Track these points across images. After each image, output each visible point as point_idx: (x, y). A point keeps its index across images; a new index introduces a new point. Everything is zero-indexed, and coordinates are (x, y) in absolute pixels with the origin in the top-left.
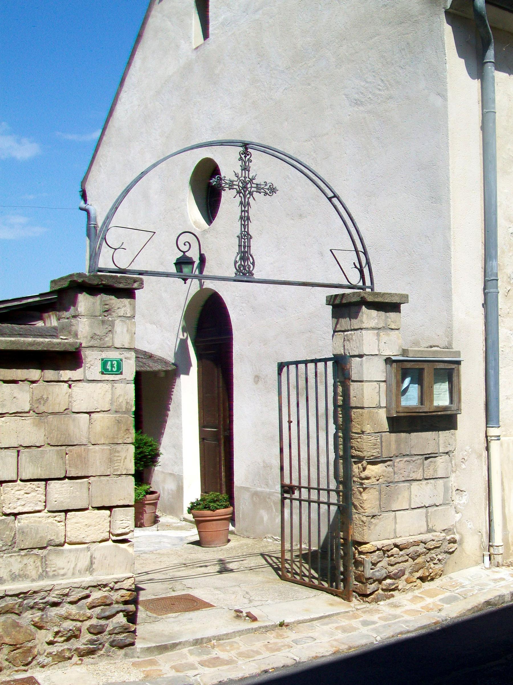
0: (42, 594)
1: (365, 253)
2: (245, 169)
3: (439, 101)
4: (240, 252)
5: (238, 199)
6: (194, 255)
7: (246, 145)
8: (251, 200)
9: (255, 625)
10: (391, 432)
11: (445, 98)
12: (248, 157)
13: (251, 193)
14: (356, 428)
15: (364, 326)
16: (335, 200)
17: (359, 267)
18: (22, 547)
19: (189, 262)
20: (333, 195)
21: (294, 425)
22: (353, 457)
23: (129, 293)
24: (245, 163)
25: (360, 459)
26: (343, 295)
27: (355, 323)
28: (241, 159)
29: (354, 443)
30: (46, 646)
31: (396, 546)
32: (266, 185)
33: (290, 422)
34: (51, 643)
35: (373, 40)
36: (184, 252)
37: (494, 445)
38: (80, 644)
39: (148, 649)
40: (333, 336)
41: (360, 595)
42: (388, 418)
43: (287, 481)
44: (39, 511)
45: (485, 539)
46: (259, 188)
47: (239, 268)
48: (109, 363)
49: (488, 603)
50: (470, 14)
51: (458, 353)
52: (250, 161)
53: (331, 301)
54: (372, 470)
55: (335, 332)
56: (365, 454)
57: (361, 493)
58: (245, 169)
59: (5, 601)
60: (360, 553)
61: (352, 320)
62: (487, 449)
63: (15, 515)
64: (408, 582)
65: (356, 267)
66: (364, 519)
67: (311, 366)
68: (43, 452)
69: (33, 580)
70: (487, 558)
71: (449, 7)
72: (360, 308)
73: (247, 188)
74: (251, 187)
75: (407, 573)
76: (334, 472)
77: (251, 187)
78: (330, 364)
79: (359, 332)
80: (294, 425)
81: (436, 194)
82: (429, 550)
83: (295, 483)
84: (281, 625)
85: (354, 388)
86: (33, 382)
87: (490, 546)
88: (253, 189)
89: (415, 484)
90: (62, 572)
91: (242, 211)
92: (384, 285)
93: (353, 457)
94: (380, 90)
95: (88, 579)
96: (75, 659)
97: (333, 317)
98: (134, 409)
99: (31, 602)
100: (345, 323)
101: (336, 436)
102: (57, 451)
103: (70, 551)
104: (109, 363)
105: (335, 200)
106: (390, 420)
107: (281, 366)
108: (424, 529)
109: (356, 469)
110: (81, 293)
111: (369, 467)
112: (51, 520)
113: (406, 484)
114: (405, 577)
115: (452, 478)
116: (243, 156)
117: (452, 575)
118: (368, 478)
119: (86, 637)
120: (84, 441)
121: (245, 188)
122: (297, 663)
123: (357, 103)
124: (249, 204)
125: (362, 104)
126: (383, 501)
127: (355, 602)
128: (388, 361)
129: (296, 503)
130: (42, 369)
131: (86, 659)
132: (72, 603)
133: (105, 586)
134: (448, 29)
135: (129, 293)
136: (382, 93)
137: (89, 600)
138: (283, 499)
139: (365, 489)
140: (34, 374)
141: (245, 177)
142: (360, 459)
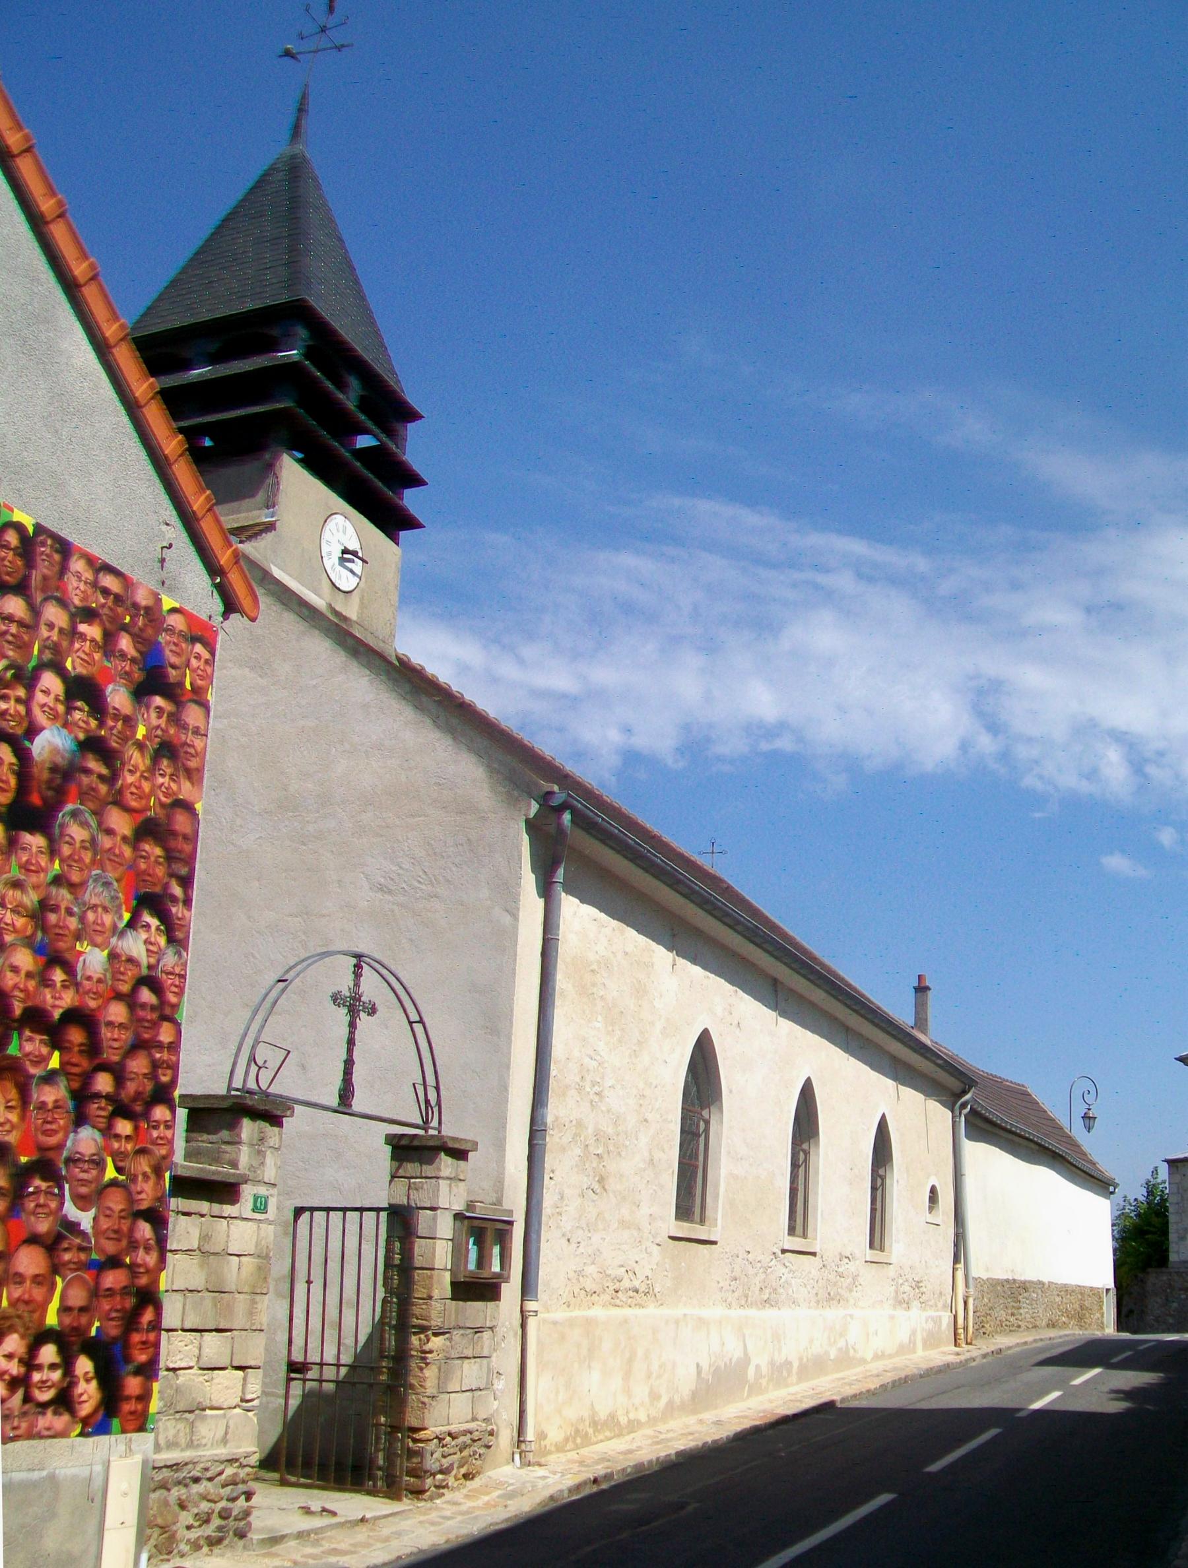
0: (190, 1466)
1: (437, 1088)
2: (357, 984)
3: (507, 919)
9: (334, 1520)
10: (452, 1299)
11: (515, 917)
14: (419, 1292)
15: (442, 1174)
16: (418, 1028)
18: (178, 1409)
20: (417, 1019)
21: (316, 1288)
22: (414, 1327)
23: (275, 1120)
25: (423, 1329)
26: (416, 1135)
27: (428, 1170)
29: (416, 1310)
30: (185, 1532)
31: (450, 1434)
33: (309, 1282)
34: (189, 1528)
35: (417, 819)
37: (532, 1323)
38: (209, 1530)
39: (263, 1540)
40: (390, 1182)
41: (412, 1492)
42: (453, 1284)
43: (298, 1357)
44: (191, 1368)
45: (515, 1434)
49: (552, 1498)
50: (552, 829)
51: (510, 1212)
53: (391, 1140)
54: (436, 1342)
55: (393, 1177)
56: (433, 1323)
57: (421, 1369)
60: (415, 1441)
61: (424, 1167)
62: (523, 1326)
63: (174, 1370)
64: (457, 1479)
66: (426, 1400)
67: (353, 1216)
68: (203, 1298)
69: (182, 1450)
70: (517, 1457)
71: (532, 815)
72: (437, 1155)
75: (456, 1466)
78: (383, 1215)
79: (433, 1181)
80: (316, 1288)
81: (495, 1026)
82: (474, 1441)
83: (314, 1357)
84: (363, 1520)
85: (419, 1246)
86: (202, 1216)
87: (519, 1441)
89: (467, 1361)
90: (204, 1441)
92: (452, 1128)
93: (414, 1327)
95: (223, 1452)
96: (205, 1549)
97: (393, 1158)
99: (181, 1475)
100: (411, 1168)
101: (384, 1301)
102: (214, 1298)
103: (212, 1416)
106: (455, 1285)
107: (299, 1212)
108: (470, 1417)
109: (415, 1340)
111: (433, 1338)
112: (201, 1379)
113: (459, 1362)
114: (454, 1472)
115: (494, 1359)
117: (489, 1473)
118: (431, 1352)
119: (216, 1521)
120: (233, 1288)
122: (421, 1551)
123: (382, 888)
125: (390, 892)
126: (442, 1380)
127: (406, 1504)
130: (211, 1201)
131: (216, 1550)
132: (210, 1479)
133: (237, 1460)
134: (526, 838)
135: (275, 1120)
136: (423, 887)
137: (223, 1477)
138: (289, 1380)
139: (427, 1364)
140: (204, 1206)
142: (423, 1329)
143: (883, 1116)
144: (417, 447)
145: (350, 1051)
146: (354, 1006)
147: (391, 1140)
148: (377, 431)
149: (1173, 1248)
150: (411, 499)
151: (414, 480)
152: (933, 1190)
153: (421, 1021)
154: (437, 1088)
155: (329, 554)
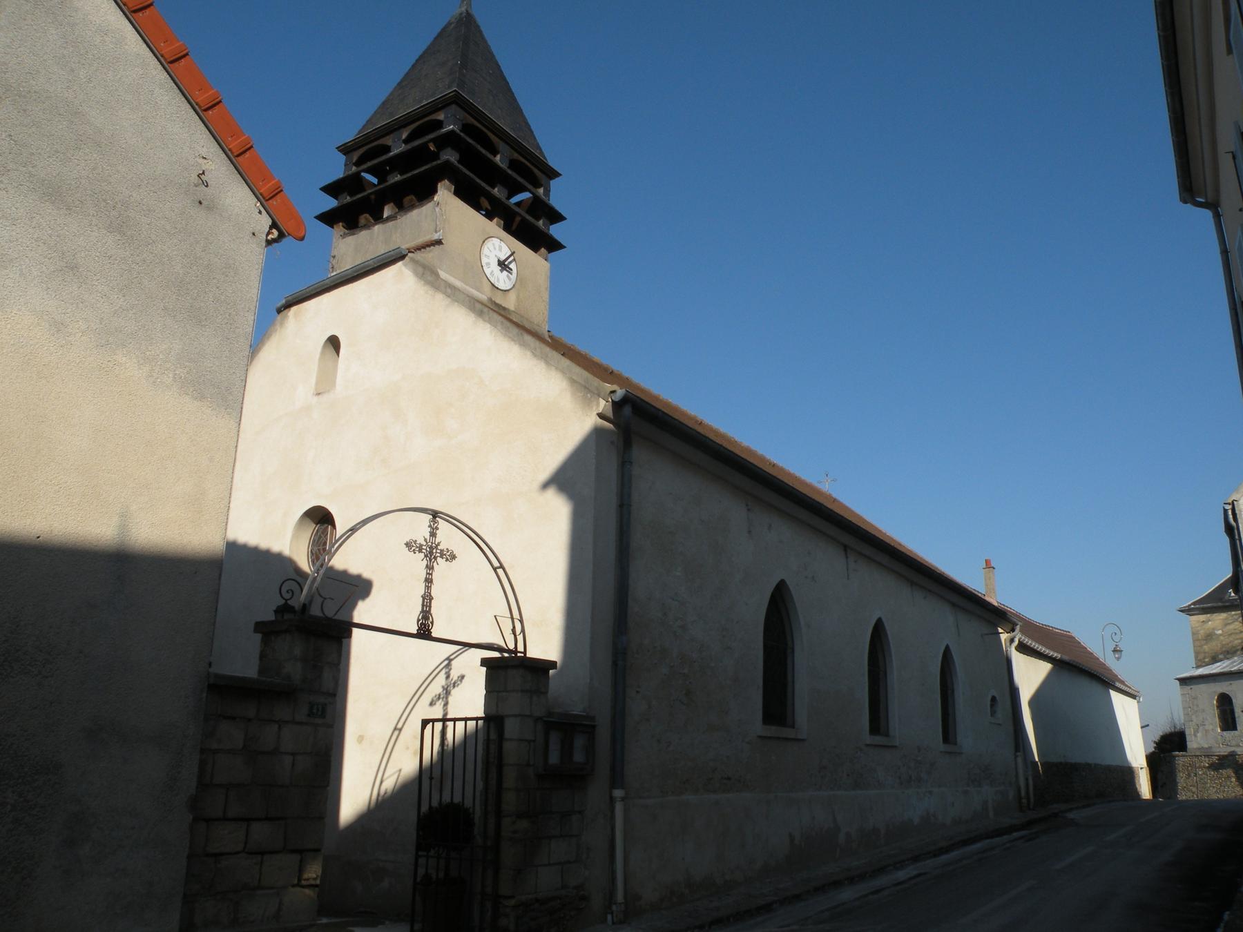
1: (521, 621)
2: (433, 534)
4: (423, 611)
5: (425, 562)
7: (435, 514)
13: (435, 558)
16: (500, 571)
52: (437, 528)
53: (484, 662)
58: (433, 534)
59: (488, 264)
76: (870, 672)
105: (500, 571)
110: (450, 181)
121: (431, 553)
128: (537, 719)
143: (947, 648)
144: (558, 195)
145: (428, 588)
146: (432, 553)
147: (484, 662)
148: (530, 187)
149: (1181, 778)
150: (556, 231)
151: (556, 217)
152: (994, 699)
153: (502, 567)
154: (521, 621)
155: (488, 264)
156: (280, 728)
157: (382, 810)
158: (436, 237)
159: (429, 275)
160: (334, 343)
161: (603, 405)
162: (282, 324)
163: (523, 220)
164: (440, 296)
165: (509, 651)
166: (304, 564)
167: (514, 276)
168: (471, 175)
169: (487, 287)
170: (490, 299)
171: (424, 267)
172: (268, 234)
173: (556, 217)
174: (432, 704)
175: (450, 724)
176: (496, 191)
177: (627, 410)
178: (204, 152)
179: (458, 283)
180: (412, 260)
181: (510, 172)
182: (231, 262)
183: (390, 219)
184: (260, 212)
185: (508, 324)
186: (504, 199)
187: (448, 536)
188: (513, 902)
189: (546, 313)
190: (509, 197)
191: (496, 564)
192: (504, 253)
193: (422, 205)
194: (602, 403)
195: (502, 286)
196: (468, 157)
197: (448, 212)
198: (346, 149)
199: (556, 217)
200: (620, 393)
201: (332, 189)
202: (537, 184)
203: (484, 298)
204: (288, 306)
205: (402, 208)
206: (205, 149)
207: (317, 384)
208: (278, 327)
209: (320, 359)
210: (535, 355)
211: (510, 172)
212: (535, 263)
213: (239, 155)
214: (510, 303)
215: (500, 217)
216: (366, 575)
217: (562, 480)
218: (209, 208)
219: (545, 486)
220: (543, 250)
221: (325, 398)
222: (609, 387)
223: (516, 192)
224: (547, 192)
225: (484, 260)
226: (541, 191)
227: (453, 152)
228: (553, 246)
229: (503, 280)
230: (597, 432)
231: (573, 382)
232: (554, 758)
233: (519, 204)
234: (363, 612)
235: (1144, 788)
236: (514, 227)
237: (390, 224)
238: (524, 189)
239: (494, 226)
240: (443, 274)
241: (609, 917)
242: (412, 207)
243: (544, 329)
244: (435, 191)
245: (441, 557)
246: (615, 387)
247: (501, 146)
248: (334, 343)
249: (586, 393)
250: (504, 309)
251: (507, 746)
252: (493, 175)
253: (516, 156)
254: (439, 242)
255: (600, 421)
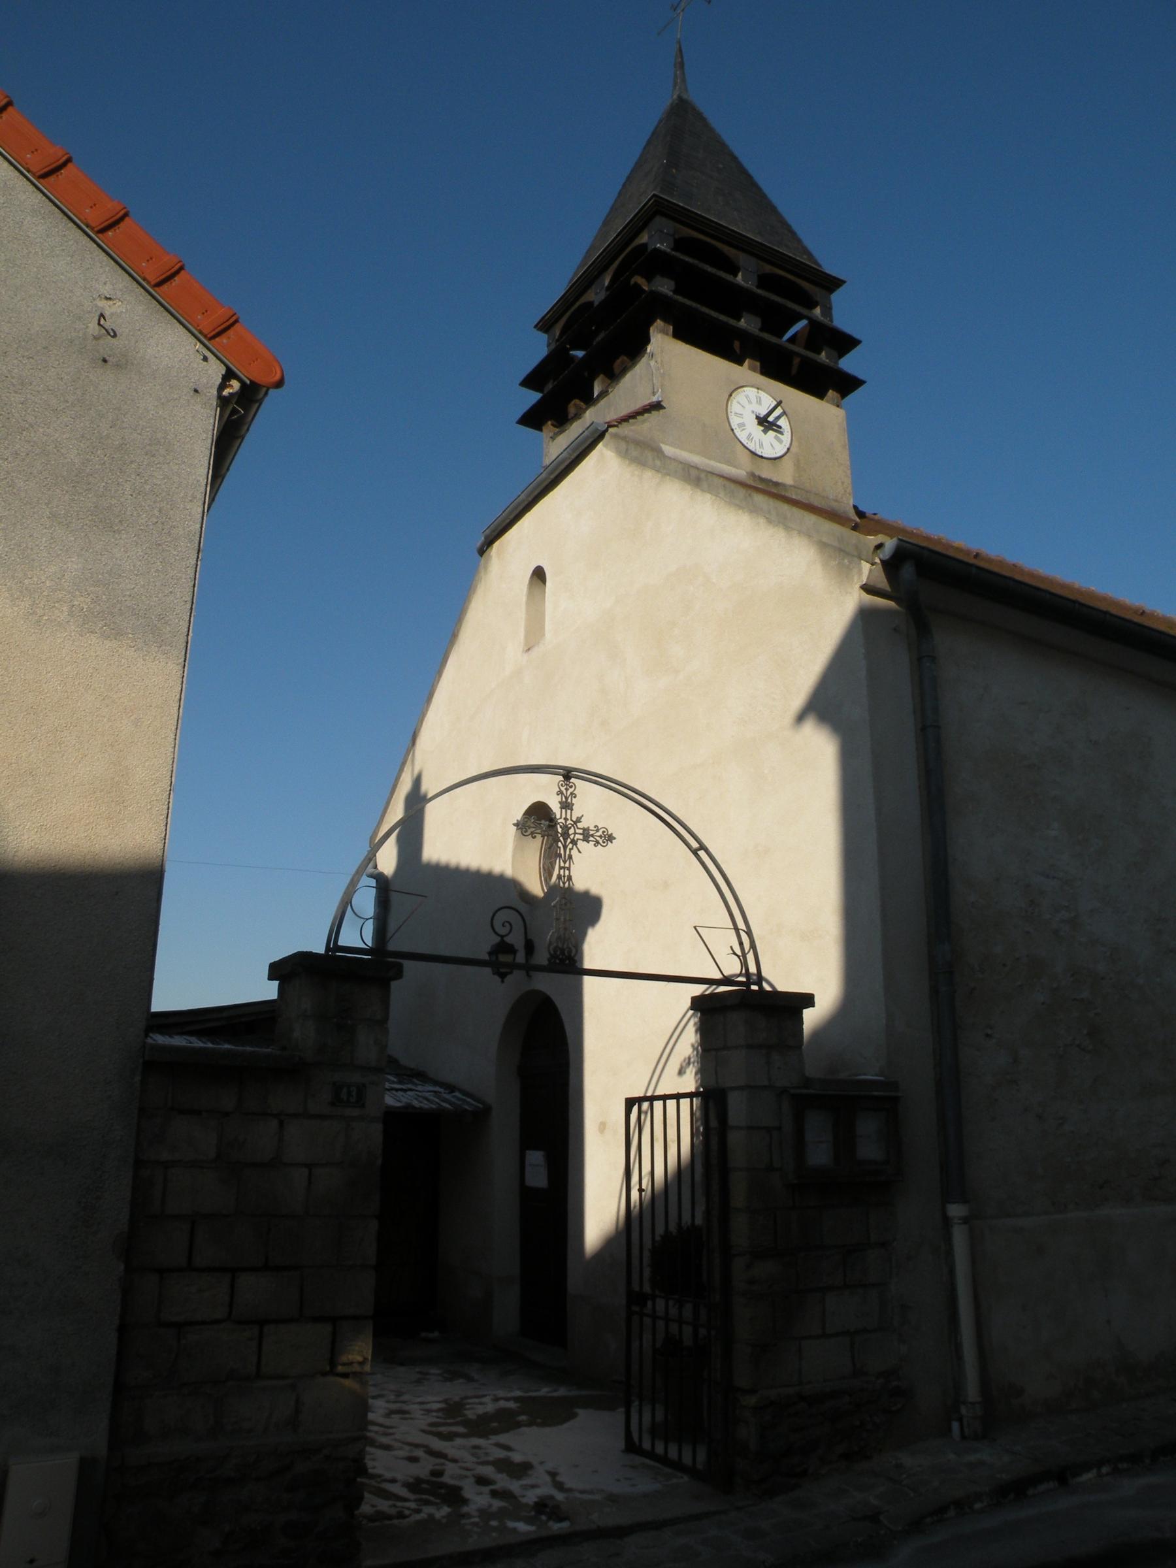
1: (749, 933)
6: (516, 939)
7: (568, 774)
8: (574, 852)
12: (571, 790)
13: (574, 842)
16: (702, 853)
17: (739, 953)
19: (510, 949)
24: (566, 798)
28: (560, 793)
32: (597, 831)
36: (502, 937)
46: (586, 835)
47: (555, 950)
48: (345, 1090)
59: (742, 425)
65: (735, 954)
73: (569, 835)
74: (575, 833)
77: (575, 833)
88: (577, 836)
91: (569, 869)
94: (774, 699)
98: (379, 1162)
104: (345, 1090)
105: (702, 853)
107: (630, 1103)
110: (665, 320)
116: (563, 789)
124: (570, 857)
129: (647, 1321)
141: (566, 819)
144: (843, 312)
148: (805, 312)
150: (849, 363)
153: (702, 847)
156: (281, 1124)
157: (610, 1244)
158: (655, 399)
159: (645, 454)
160: (539, 575)
161: (866, 571)
162: (486, 568)
163: (805, 362)
164: (649, 474)
165: (726, 981)
166: (536, 888)
167: (786, 438)
168: (694, 305)
169: (744, 458)
170: (752, 475)
171: (638, 443)
172: (222, 387)
173: (845, 343)
174: (681, 1072)
175: (672, 1104)
176: (742, 323)
177: (908, 571)
178: (106, 290)
179: (696, 459)
180: (615, 436)
181: (759, 291)
182: (159, 435)
183: (604, 394)
184: (205, 359)
185: (785, 507)
186: (832, 364)
187: (592, 805)
188: (752, 1400)
189: (848, 481)
190: (781, 336)
191: (695, 845)
192: (765, 403)
193: (634, 364)
194: (866, 567)
195: (768, 452)
196: (687, 281)
197: (671, 365)
198: (545, 325)
199: (845, 343)
200: (890, 544)
201: (531, 381)
202: (812, 305)
203: (740, 473)
204: (490, 542)
205: (614, 376)
206: (109, 287)
207: (526, 637)
208: (482, 574)
209: (527, 604)
210: (769, 521)
211: (759, 291)
212: (825, 414)
213: (162, 283)
214: (785, 475)
215: (753, 358)
216: (595, 890)
217: (822, 706)
218: (118, 366)
219: (800, 718)
220: (831, 393)
221: (536, 652)
222: (872, 540)
223: (784, 326)
224: (827, 311)
225: (735, 421)
226: (817, 311)
227: (666, 280)
228: (846, 385)
229: (770, 445)
230: (864, 616)
231: (823, 546)
232: (820, 1154)
233: (792, 340)
234: (598, 949)
235: (423, 1334)
236: (794, 371)
237: (603, 402)
238: (798, 317)
239: (744, 372)
240: (668, 450)
241: (955, 1425)
242: (624, 371)
243: (847, 504)
244: (647, 341)
245: (586, 839)
246: (880, 538)
247: (742, 259)
248: (539, 575)
249: (839, 557)
250: (776, 484)
251: (735, 1139)
252: (737, 301)
253: (768, 268)
254: (657, 406)
255: (869, 599)
